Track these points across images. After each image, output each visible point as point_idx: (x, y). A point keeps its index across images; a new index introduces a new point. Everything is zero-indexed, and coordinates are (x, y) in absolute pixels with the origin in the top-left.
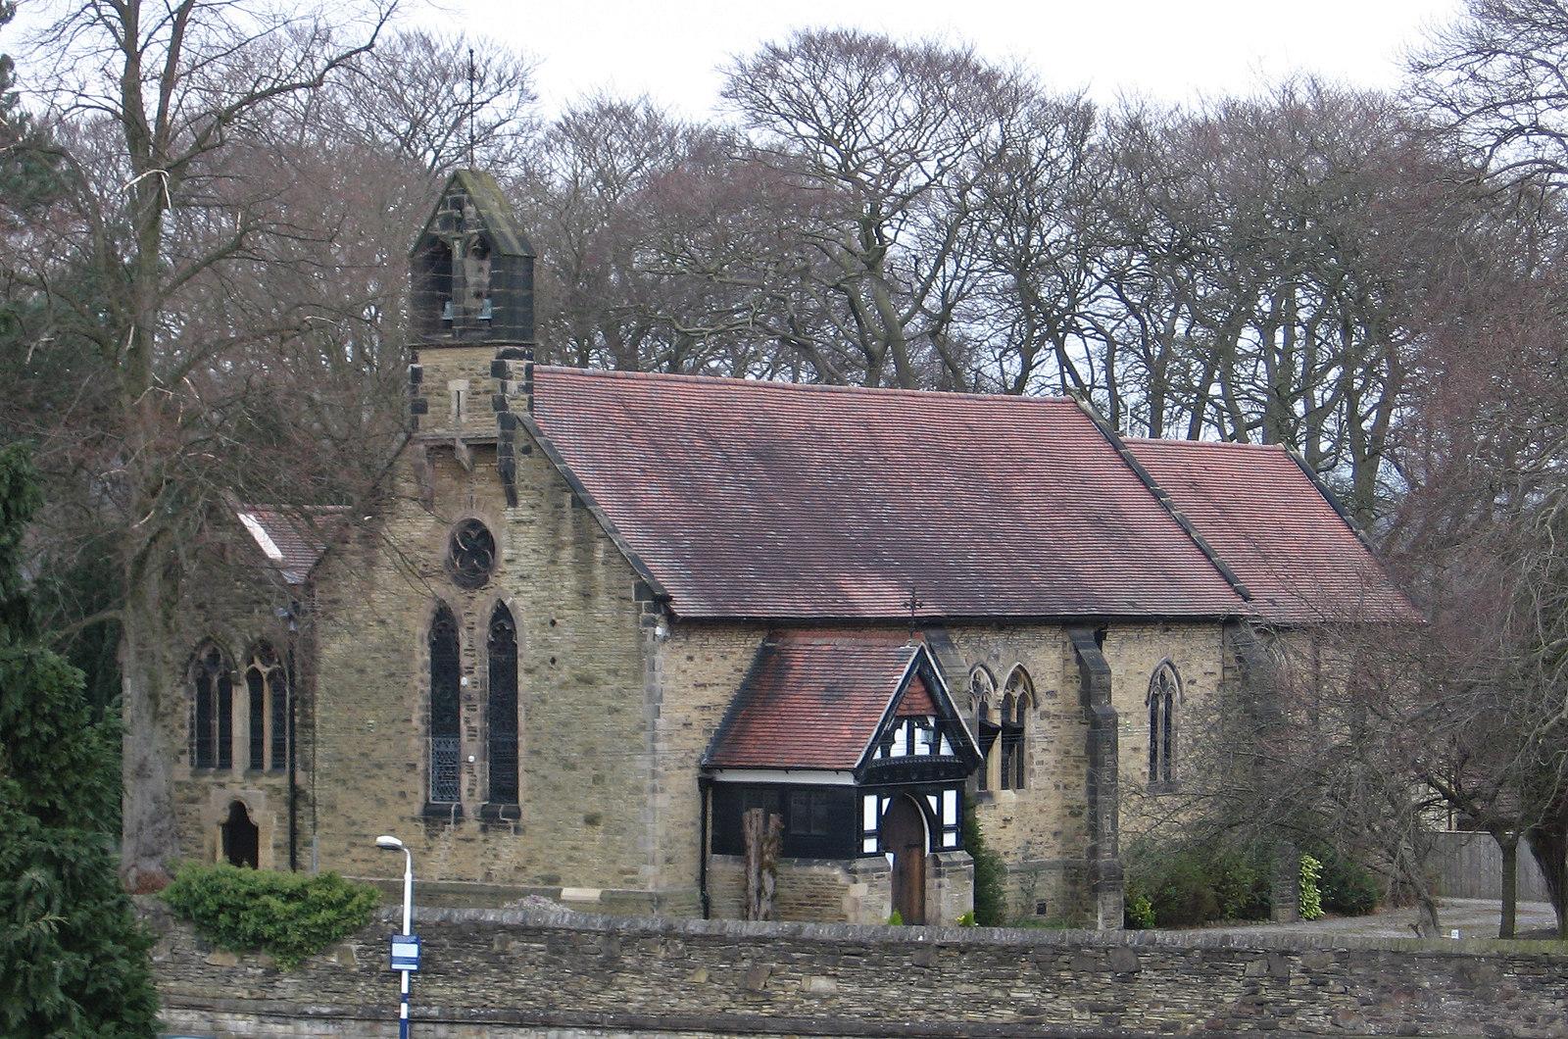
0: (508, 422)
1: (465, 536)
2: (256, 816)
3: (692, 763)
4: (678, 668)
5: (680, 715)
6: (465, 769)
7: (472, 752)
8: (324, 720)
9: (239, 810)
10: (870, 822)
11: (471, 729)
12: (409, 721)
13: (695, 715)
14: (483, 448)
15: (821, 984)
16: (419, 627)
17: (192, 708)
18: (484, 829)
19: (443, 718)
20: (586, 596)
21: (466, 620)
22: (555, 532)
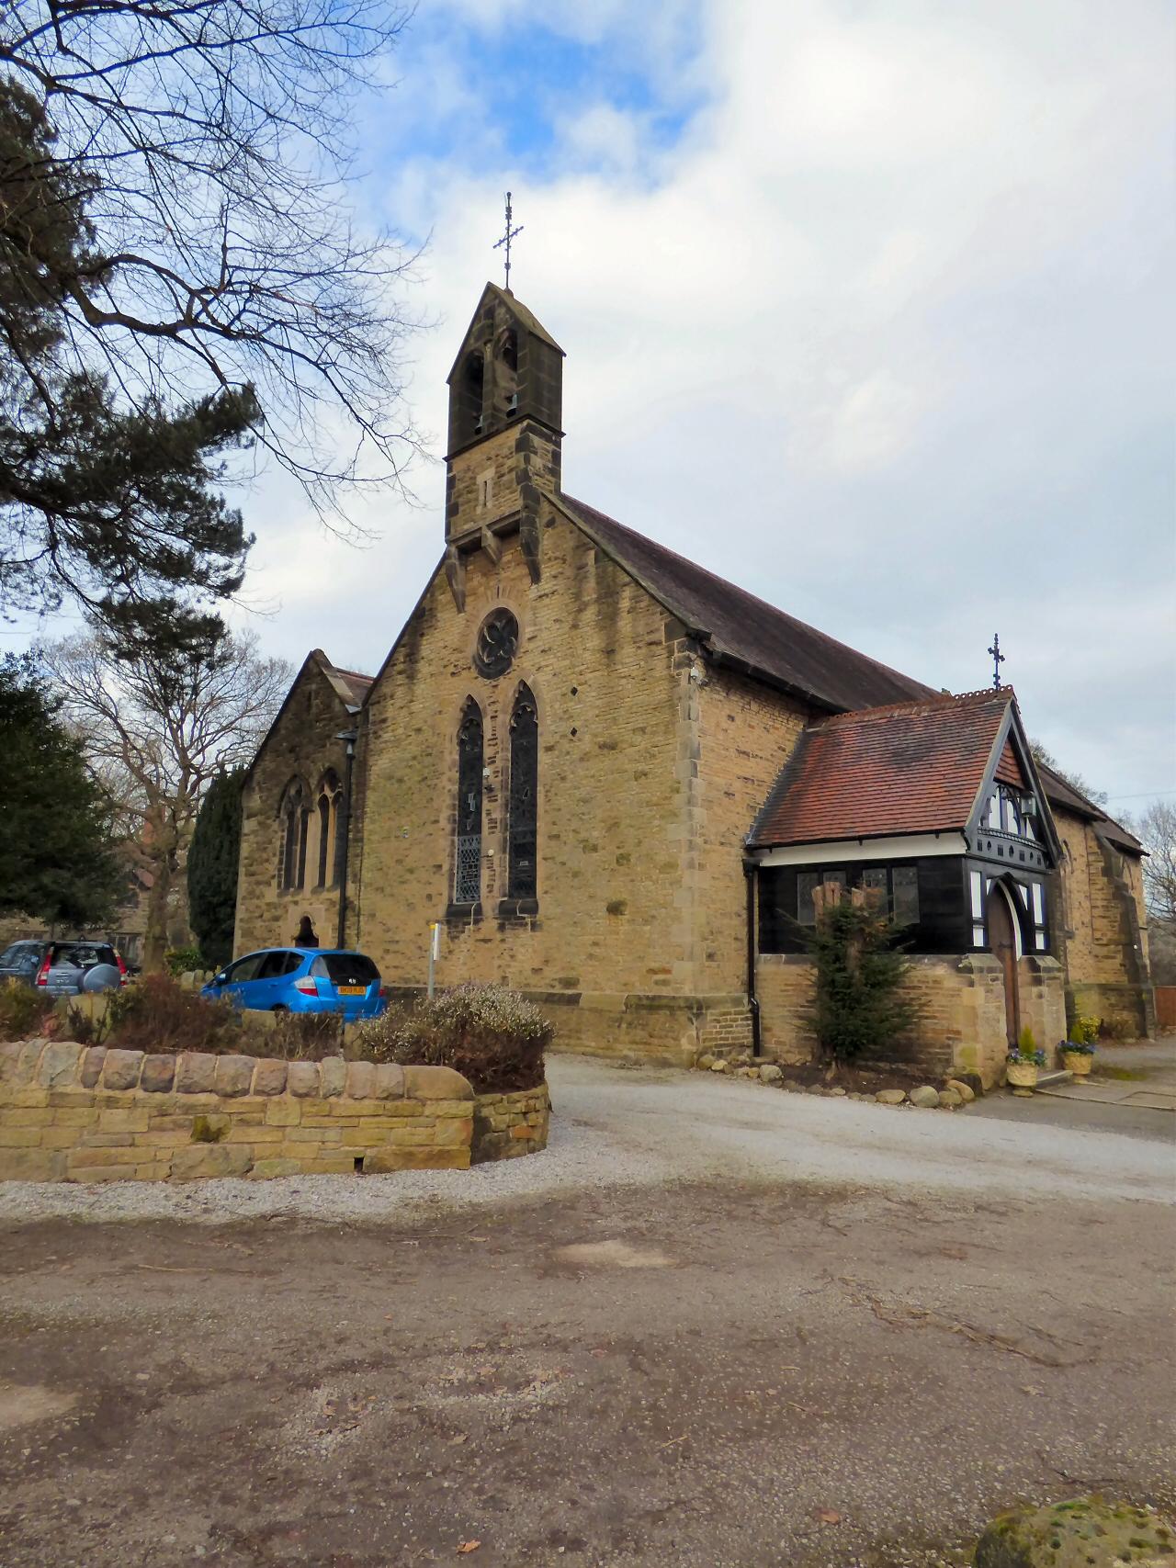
1: (491, 627)
3: (736, 841)
4: (718, 725)
5: (720, 781)
6: (484, 863)
9: (306, 923)
10: (977, 912)
18: (502, 928)
22: (577, 596)
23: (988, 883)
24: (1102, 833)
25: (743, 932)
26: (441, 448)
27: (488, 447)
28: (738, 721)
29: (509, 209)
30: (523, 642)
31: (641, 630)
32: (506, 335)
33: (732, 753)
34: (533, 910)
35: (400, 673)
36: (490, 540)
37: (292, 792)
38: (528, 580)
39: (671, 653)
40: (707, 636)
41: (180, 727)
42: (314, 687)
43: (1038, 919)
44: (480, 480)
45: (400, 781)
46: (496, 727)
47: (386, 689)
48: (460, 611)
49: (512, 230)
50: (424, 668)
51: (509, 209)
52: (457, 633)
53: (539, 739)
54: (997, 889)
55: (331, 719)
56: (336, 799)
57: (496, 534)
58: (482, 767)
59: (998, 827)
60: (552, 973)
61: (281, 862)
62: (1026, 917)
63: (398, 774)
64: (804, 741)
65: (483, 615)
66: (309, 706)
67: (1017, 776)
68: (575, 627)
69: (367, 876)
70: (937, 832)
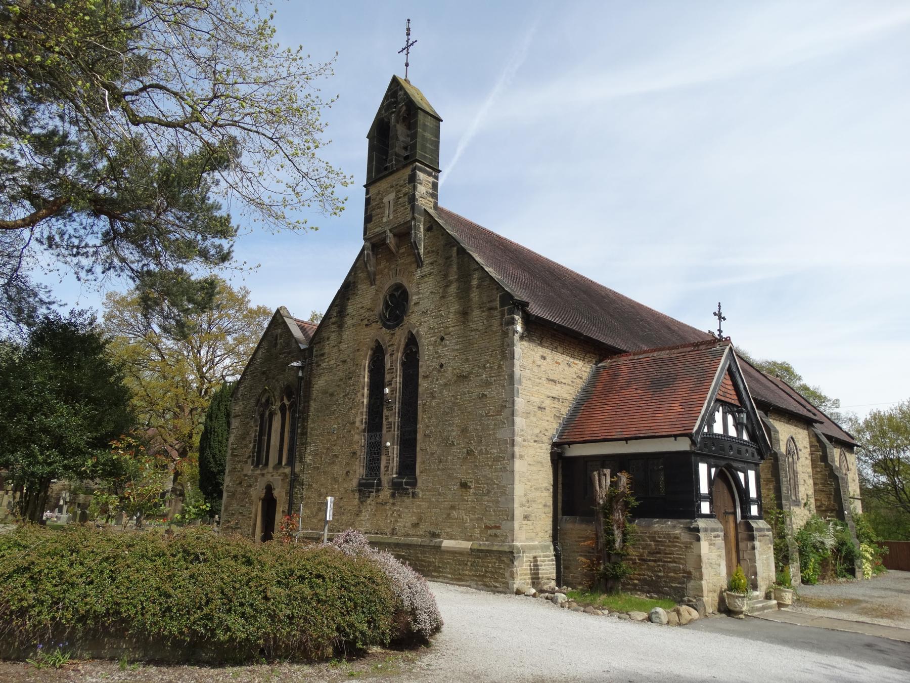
1: (392, 296)
2: (276, 493)
3: (545, 439)
4: (534, 362)
5: (536, 400)
6: (384, 452)
8: (312, 429)
9: (269, 489)
10: (704, 489)
11: (390, 423)
12: (354, 423)
13: (548, 403)
17: (256, 431)
18: (393, 495)
20: (465, 314)
21: (390, 350)
22: (446, 276)
23: (713, 470)
24: (819, 431)
25: (550, 502)
26: (362, 178)
27: (391, 180)
28: (549, 359)
29: (408, 29)
30: (412, 308)
31: (485, 299)
32: (404, 108)
33: (544, 381)
34: (414, 484)
35: (333, 323)
36: (391, 240)
37: (263, 400)
38: (414, 266)
39: (503, 315)
40: (527, 304)
41: (199, 352)
42: (279, 331)
43: (753, 494)
44: (385, 200)
45: (332, 395)
46: (394, 362)
47: (325, 335)
48: (372, 285)
49: (410, 42)
50: (349, 322)
51: (408, 29)
52: (369, 298)
53: (420, 370)
54: (720, 474)
55: (289, 353)
56: (291, 406)
57: (395, 235)
58: (383, 388)
59: (722, 433)
60: (424, 527)
61: (254, 447)
62: (744, 492)
63: (331, 391)
64: (596, 375)
65: (387, 287)
66: (276, 344)
67: (736, 398)
68: (443, 297)
69: (308, 459)
70: (676, 436)
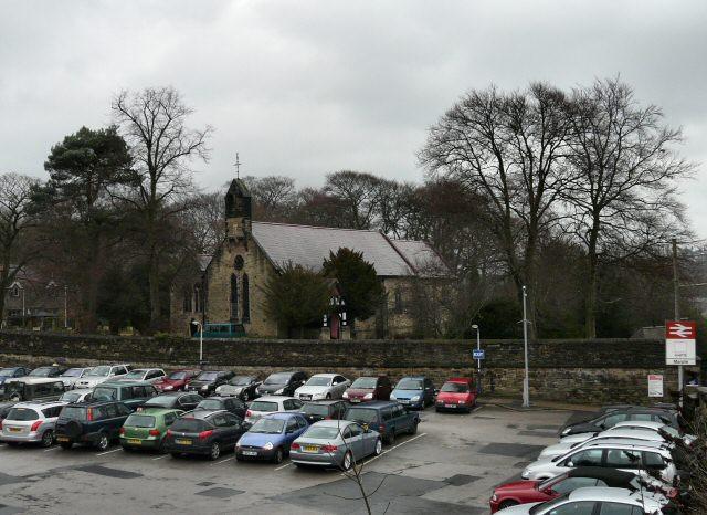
0: (245, 233)
7: (239, 305)
14: (240, 239)
15: (295, 354)
16: (228, 279)
19: (234, 299)
20: (262, 271)
